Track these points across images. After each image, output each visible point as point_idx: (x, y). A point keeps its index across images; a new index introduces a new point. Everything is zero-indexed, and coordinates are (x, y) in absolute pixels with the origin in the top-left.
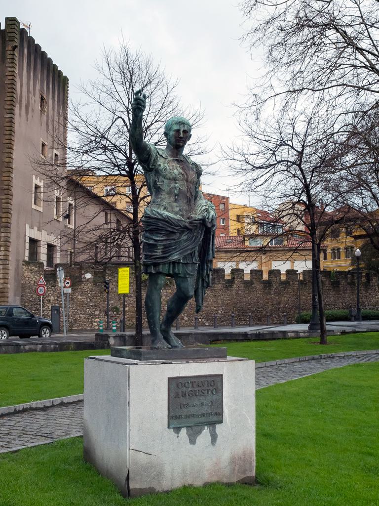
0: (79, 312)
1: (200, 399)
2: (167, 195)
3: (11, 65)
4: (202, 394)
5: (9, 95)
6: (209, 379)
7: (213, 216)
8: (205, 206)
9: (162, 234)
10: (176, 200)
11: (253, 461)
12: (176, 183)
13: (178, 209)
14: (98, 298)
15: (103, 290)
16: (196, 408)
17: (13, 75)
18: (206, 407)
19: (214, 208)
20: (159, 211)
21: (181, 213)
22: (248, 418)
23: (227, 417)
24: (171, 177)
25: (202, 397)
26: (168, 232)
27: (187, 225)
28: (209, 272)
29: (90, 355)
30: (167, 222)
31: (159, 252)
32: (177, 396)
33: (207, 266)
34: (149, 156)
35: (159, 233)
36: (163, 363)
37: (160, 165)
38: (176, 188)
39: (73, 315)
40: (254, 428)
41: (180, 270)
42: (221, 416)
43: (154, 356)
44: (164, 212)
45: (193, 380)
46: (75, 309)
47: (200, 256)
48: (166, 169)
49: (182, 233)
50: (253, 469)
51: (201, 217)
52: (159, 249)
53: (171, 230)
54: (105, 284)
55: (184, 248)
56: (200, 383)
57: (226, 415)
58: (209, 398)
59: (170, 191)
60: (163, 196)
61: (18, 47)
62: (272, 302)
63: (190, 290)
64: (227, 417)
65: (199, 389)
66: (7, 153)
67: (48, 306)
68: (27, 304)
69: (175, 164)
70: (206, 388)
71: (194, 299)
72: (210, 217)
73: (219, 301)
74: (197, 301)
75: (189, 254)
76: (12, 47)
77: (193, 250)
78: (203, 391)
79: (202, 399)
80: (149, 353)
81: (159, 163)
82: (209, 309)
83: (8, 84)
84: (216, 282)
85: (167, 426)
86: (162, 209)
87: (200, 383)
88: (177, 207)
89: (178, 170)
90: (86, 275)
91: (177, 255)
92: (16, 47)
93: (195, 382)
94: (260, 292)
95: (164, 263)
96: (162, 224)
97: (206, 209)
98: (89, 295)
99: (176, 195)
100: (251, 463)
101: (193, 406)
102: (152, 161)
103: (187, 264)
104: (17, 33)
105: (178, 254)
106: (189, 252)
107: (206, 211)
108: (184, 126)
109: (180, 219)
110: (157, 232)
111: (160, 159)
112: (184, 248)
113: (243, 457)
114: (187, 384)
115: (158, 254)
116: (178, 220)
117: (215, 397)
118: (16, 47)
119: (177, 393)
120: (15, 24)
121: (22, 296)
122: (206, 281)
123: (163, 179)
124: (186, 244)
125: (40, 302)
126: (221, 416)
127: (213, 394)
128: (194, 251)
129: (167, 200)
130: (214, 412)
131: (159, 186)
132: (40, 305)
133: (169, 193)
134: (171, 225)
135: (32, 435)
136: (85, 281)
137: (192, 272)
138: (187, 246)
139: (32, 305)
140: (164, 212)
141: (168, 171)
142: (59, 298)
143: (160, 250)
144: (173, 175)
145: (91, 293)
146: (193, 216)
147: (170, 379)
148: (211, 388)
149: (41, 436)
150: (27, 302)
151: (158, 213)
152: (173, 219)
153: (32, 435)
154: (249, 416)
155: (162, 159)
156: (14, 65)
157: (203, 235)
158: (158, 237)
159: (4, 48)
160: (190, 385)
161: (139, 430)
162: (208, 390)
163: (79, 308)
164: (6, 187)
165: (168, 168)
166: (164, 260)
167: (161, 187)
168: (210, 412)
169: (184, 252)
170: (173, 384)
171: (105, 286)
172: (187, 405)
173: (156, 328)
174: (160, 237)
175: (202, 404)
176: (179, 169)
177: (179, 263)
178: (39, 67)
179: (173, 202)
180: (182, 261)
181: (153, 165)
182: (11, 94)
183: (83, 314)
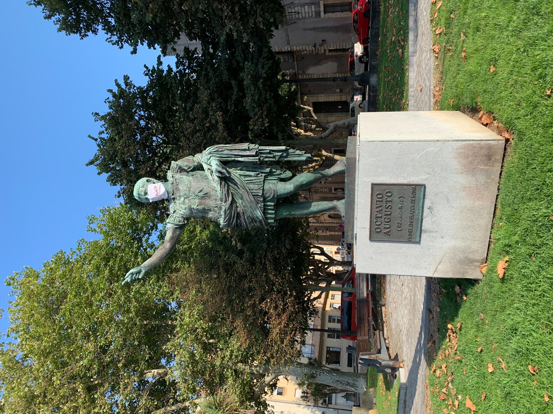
6: (375, 199)
22: (425, 151)
32: (387, 234)
45: (374, 216)
57: (417, 179)
116: (225, 214)
119: (385, 233)
122: (281, 156)
127: (390, 221)
147: (371, 239)
152: (225, 219)
175: (401, 208)
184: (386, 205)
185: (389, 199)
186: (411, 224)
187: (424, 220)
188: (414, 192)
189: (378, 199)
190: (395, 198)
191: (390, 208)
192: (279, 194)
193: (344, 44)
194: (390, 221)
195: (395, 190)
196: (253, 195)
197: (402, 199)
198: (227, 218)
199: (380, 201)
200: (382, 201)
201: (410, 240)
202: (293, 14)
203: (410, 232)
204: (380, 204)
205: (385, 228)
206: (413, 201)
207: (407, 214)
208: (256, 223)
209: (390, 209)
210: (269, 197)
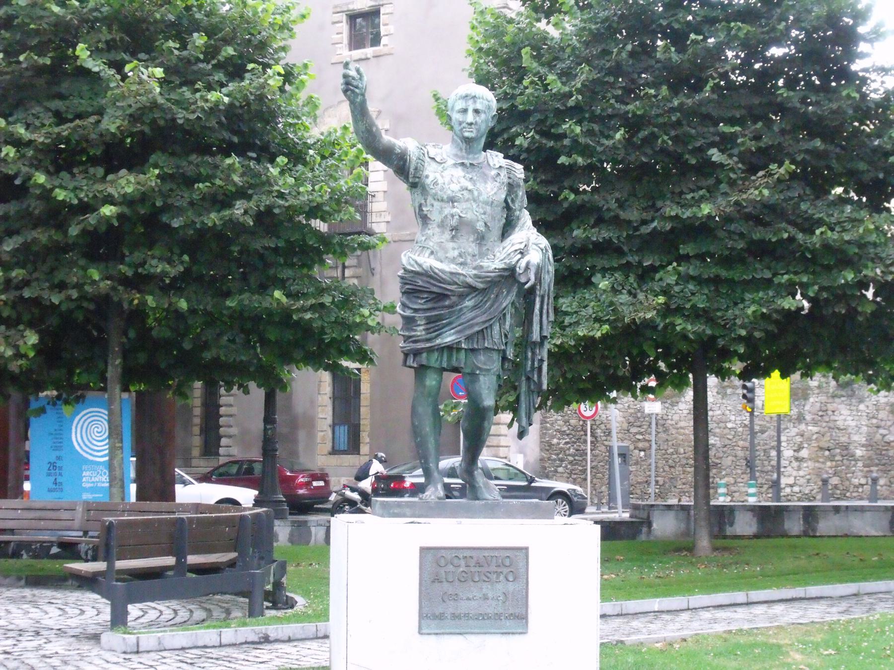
1: (481, 588)
2: (437, 230)
9: (423, 298)
10: (453, 237)
12: (454, 207)
13: (456, 253)
14: (730, 425)
15: (740, 407)
16: (473, 603)
18: (494, 603)
21: (461, 260)
25: (485, 585)
26: (434, 296)
27: (469, 280)
30: (431, 277)
31: (421, 331)
33: (533, 353)
34: (406, 160)
35: (418, 298)
36: (412, 523)
37: (427, 177)
38: (453, 216)
39: (667, 468)
41: (461, 359)
46: (672, 454)
48: (436, 183)
49: (462, 297)
51: (502, 266)
52: (419, 325)
55: (468, 321)
58: (499, 586)
59: (442, 221)
60: (433, 229)
63: (484, 396)
65: (479, 569)
69: (459, 172)
70: (493, 568)
75: (478, 332)
77: (487, 325)
78: (489, 575)
79: (486, 588)
81: (426, 173)
85: (417, 630)
86: (427, 255)
88: (454, 249)
91: (450, 335)
93: (472, 557)
95: (430, 350)
99: (454, 229)
101: (468, 599)
102: (412, 170)
103: (473, 350)
105: (454, 334)
106: (477, 329)
108: (475, 102)
109: (454, 271)
110: (416, 295)
112: (468, 321)
115: (419, 334)
116: (452, 273)
117: (511, 587)
123: (433, 202)
124: (470, 315)
125: (586, 435)
127: (508, 580)
129: (436, 239)
130: (510, 612)
131: (425, 213)
132: (585, 442)
133: (442, 225)
134: (440, 282)
137: (485, 364)
138: (472, 319)
139: (566, 443)
142: (633, 426)
143: (421, 328)
144: (449, 192)
147: (424, 550)
148: (505, 570)
150: (553, 437)
151: (416, 262)
155: (434, 164)
158: (416, 303)
160: (463, 563)
165: (439, 182)
166: (428, 345)
168: (501, 611)
169: (465, 329)
170: (429, 557)
172: (455, 597)
175: (486, 598)
177: (459, 350)
180: (463, 345)
181: (414, 177)
186: (455, 617)
187: (460, 637)
192: (481, 378)
193: (233, 431)
196: (482, 330)
197: (446, 598)
198: (444, 276)
201: (422, 616)
202: (340, 270)
203: (441, 617)
206: (498, 616)
207: (472, 607)
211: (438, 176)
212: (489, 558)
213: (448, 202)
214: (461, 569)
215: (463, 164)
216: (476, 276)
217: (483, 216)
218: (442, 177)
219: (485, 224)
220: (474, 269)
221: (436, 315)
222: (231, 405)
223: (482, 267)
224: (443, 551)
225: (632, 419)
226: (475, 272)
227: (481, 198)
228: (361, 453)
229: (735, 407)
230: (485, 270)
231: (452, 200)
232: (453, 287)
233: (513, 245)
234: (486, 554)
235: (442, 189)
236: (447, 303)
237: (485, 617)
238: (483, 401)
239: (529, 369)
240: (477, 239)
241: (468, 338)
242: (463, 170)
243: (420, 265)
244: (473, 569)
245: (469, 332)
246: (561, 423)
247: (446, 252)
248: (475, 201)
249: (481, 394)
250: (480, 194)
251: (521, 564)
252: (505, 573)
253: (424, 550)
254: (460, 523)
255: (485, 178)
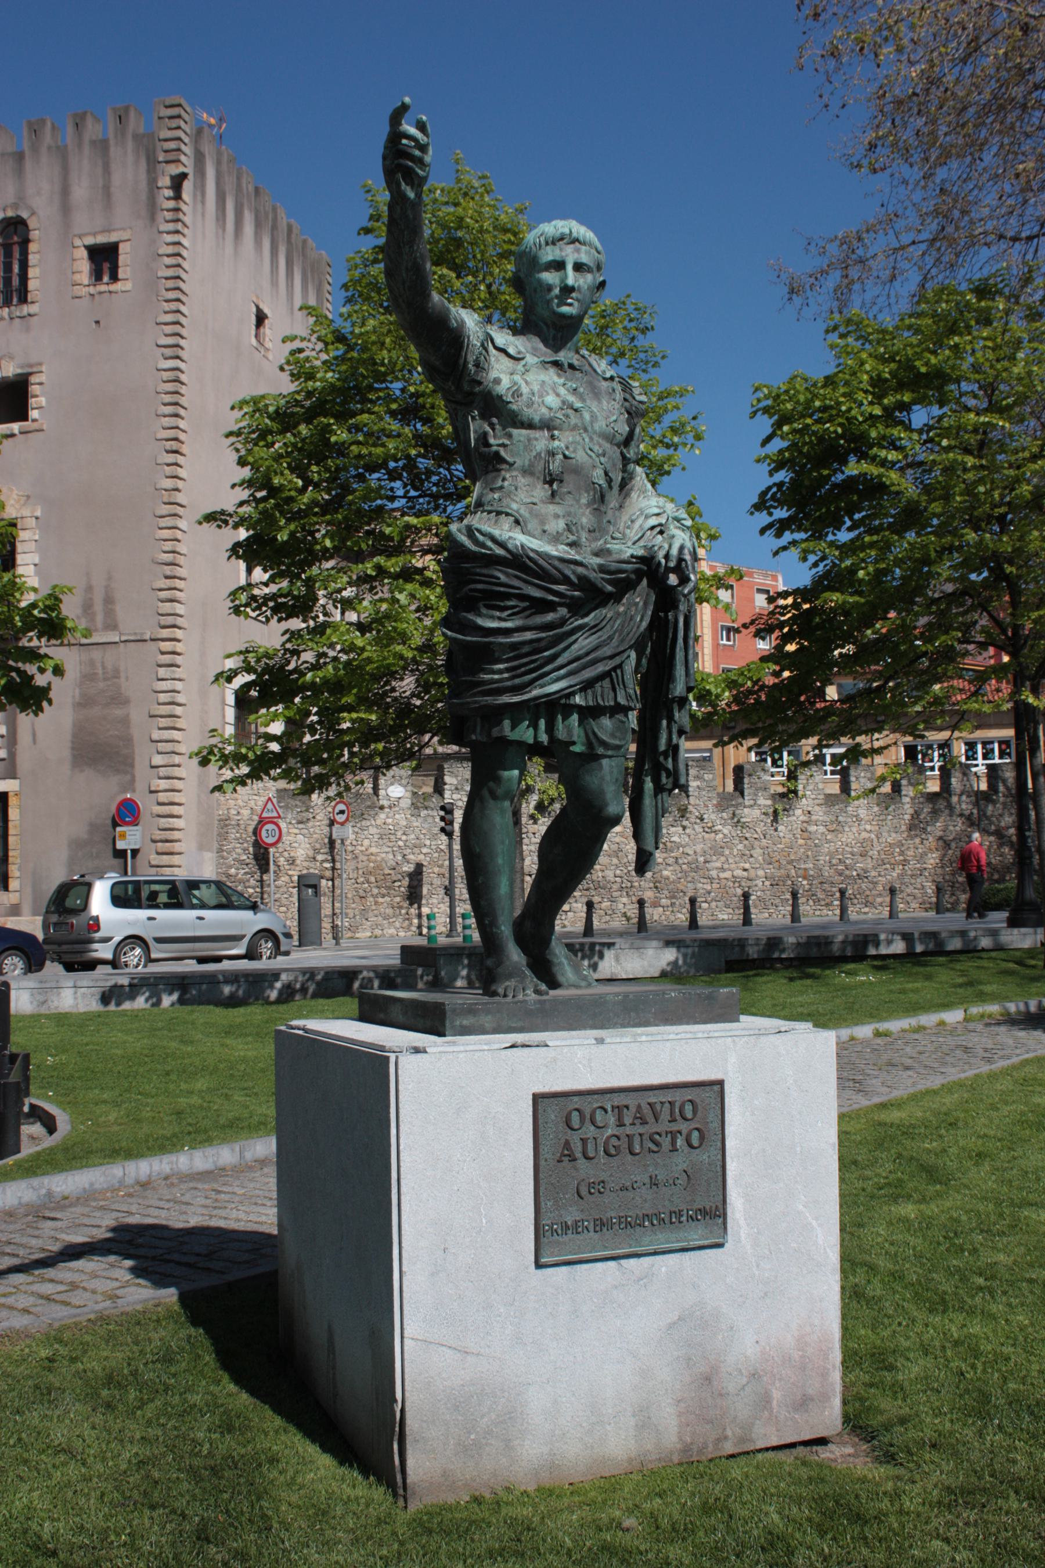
0: (375, 891)
3: (171, 227)
4: (655, 1148)
5: (167, 309)
6: (678, 1096)
7: (682, 548)
8: (657, 515)
10: (553, 494)
11: (834, 1366)
12: (553, 438)
13: (561, 525)
14: (425, 850)
15: (436, 830)
17: (179, 255)
19: (689, 523)
20: (496, 532)
21: (572, 538)
22: (814, 1223)
23: (742, 1222)
24: (537, 419)
27: (592, 575)
28: (675, 737)
29: (293, 1019)
32: (567, 1154)
36: (513, 1046)
37: (497, 381)
38: (552, 454)
40: (834, 1257)
41: (570, 729)
42: (720, 1220)
43: (487, 1020)
44: (511, 534)
45: (619, 1100)
47: (643, 684)
48: (518, 394)
50: (834, 1390)
51: (641, 552)
53: (537, 593)
54: (442, 813)
55: (587, 654)
56: (646, 1110)
61: (191, 177)
62: (902, 853)
64: (742, 1222)
65: (641, 1129)
66: (168, 465)
67: (290, 876)
68: (233, 871)
69: (551, 376)
70: (664, 1126)
71: (629, 831)
72: (674, 552)
73: (757, 852)
74: (637, 835)
76: (172, 178)
78: (657, 1137)
80: (471, 1011)
81: (493, 374)
82: (727, 874)
83: (167, 278)
84: (747, 803)
86: (506, 527)
87: (646, 1110)
88: (557, 516)
89: (558, 395)
90: (391, 789)
92: (184, 176)
93: (627, 1107)
94: (868, 827)
96: (507, 574)
97: (660, 525)
98: (401, 843)
100: (824, 1375)
101: (624, 1189)
104: (186, 140)
106: (601, 668)
107: (661, 532)
111: (498, 360)
113: (796, 1355)
114: (599, 1116)
115: (496, 677)
116: (562, 560)
118: (184, 176)
119: (567, 1144)
120: (179, 117)
121: (220, 850)
122: (667, 770)
126: (720, 1220)
127: (691, 1146)
128: (620, 666)
131: (495, 448)
133: (527, 472)
135: (154, 1258)
136: (390, 807)
140: (511, 534)
141: (524, 397)
144: (544, 410)
145: (404, 838)
146: (614, 546)
147: (537, 1099)
148: (684, 1127)
149: (179, 1263)
150: (231, 867)
153: (154, 1258)
154: (816, 1219)
156: (179, 226)
157: (649, 613)
159: (153, 186)
160: (612, 1120)
161: (432, 1274)
162: (674, 1135)
163: (372, 879)
164: (168, 557)
167: (503, 453)
169: (584, 667)
170: (552, 1113)
171: (442, 819)
173: (498, 928)
174: (500, 619)
175: (654, 1183)
176: (562, 391)
178: (249, 228)
179: (543, 502)
182: (173, 306)
183: (383, 896)
184: (660, 1135)
185: (680, 1142)
186: (601, 1225)
187: (612, 1264)
188: (704, 1212)
189: (677, 1105)
190: (681, 1161)
191: (654, 1148)
194: (691, 1146)
195: (714, 1152)
197: (584, 1192)
199: (672, 1113)
200: (673, 1120)
204: (665, 1115)
205: (584, 1141)
208: (507, 670)
209: (650, 1151)
210: (601, 727)
211: (517, 378)
212: (658, 1107)
213: (541, 428)
214: (610, 1132)
215: (556, 364)
216: (602, 569)
217: (603, 459)
218: (527, 382)
219: (606, 474)
220: (597, 554)
221: (531, 641)
222: (179, 817)
223: (609, 552)
224: (576, 1099)
225: (318, 846)
226: (598, 561)
227: (597, 427)
228: (11, 888)
229: (429, 830)
230: (615, 557)
231: (548, 426)
232: (561, 588)
233: (647, 517)
234: (652, 1100)
235: (530, 404)
236: (550, 617)
237: (655, 1220)
238: (607, 805)
239: (662, 747)
240: (594, 501)
241: (587, 686)
242: (559, 376)
243: (502, 545)
244: (629, 1130)
245: (588, 674)
246: (239, 851)
247: (543, 523)
248: (586, 430)
249: (602, 792)
250: (594, 418)
251: (713, 1116)
252: (685, 1132)
253: (537, 1099)
254: (600, 1041)
255: (597, 395)
